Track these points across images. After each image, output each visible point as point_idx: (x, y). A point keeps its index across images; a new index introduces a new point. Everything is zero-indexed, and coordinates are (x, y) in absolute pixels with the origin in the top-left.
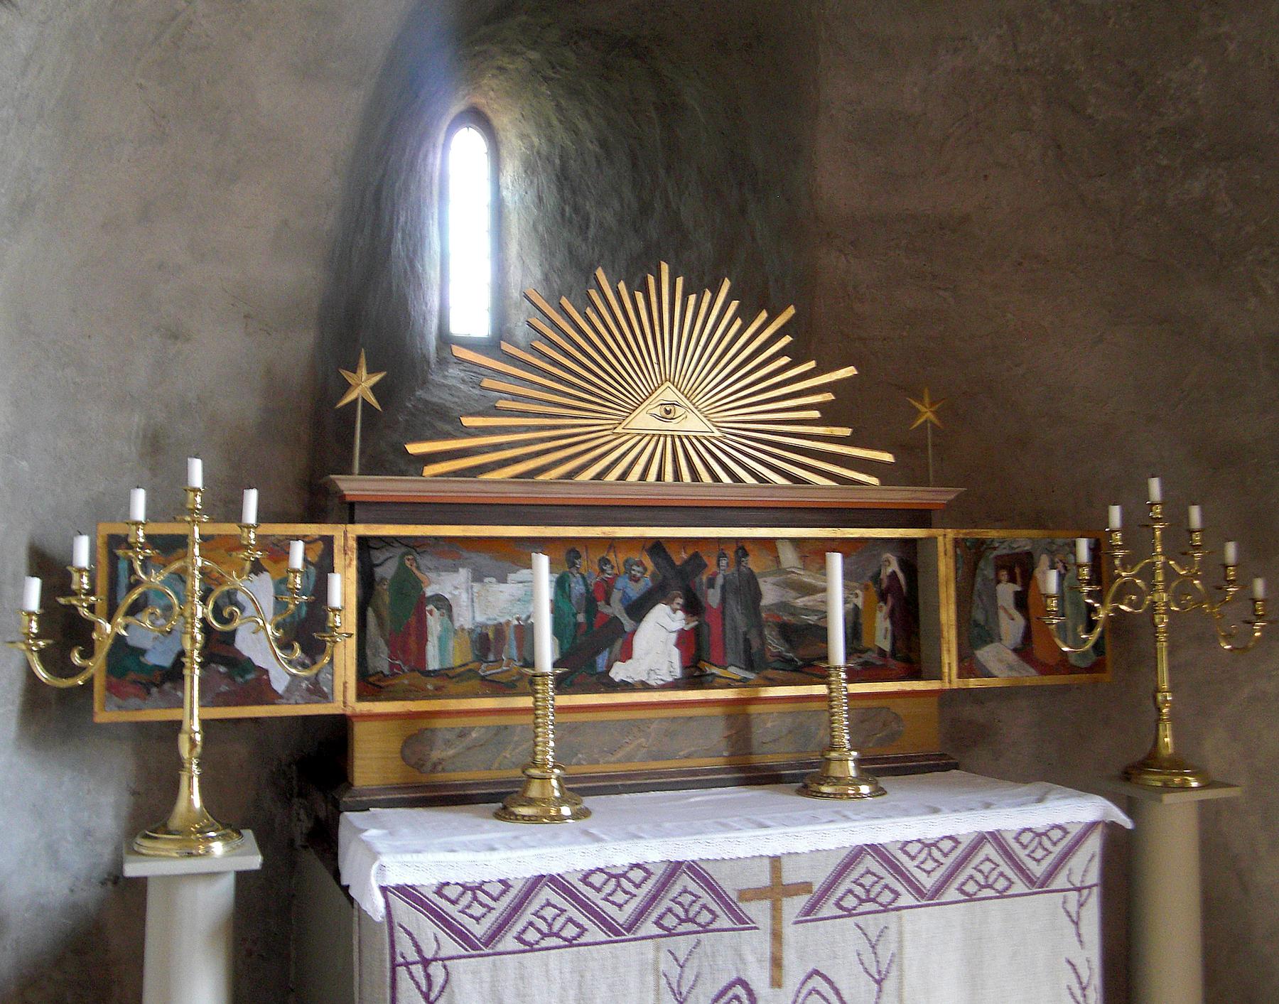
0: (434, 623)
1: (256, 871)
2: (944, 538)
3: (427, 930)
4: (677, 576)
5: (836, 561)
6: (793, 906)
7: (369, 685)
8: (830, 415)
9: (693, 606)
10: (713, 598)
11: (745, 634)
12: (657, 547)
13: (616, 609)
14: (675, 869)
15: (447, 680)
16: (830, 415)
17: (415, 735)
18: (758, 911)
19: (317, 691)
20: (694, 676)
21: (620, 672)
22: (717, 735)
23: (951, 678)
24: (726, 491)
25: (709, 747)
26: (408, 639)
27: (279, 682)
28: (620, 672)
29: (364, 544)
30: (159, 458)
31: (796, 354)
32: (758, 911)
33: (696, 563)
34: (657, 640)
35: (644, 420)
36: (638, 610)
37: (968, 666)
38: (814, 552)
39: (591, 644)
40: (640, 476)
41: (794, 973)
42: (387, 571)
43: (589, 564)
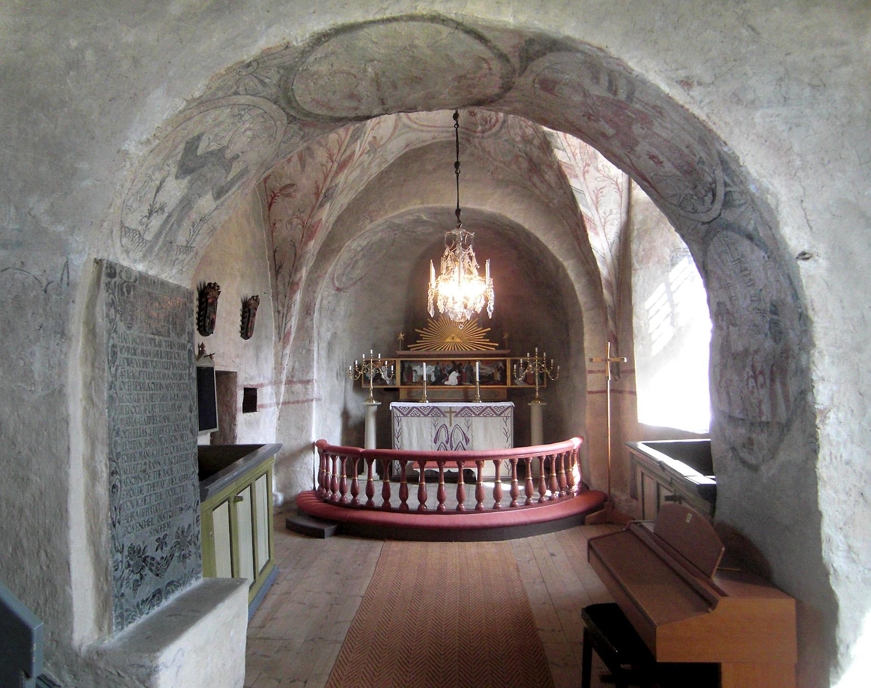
0: (414, 374)
1: (653, 658)
2: (508, 360)
3: (398, 413)
4: (457, 367)
5: (477, 363)
6: (453, 414)
7: (403, 383)
8: (485, 337)
9: (460, 372)
10: (464, 370)
11: (466, 377)
12: (453, 362)
13: (446, 372)
14: (434, 407)
15: (416, 383)
16: (485, 337)
17: (409, 392)
18: (448, 415)
19: (394, 384)
20: (460, 383)
21: (446, 383)
22: (462, 394)
23: (509, 385)
24: (464, 352)
25: (461, 395)
26: (410, 377)
27: (388, 382)
28: (446, 383)
29: (402, 362)
30: (374, 347)
31: (427, 327)
32: (448, 415)
33: (461, 364)
34: (453, 378)
35: (449, 340)
36: (450, 372)
37: (513, 383)
38: (476, 361)
39: (441, 378)
40: (449, 350)
41: (453, 425)
42: (406, 366)
43: (440, 364)
